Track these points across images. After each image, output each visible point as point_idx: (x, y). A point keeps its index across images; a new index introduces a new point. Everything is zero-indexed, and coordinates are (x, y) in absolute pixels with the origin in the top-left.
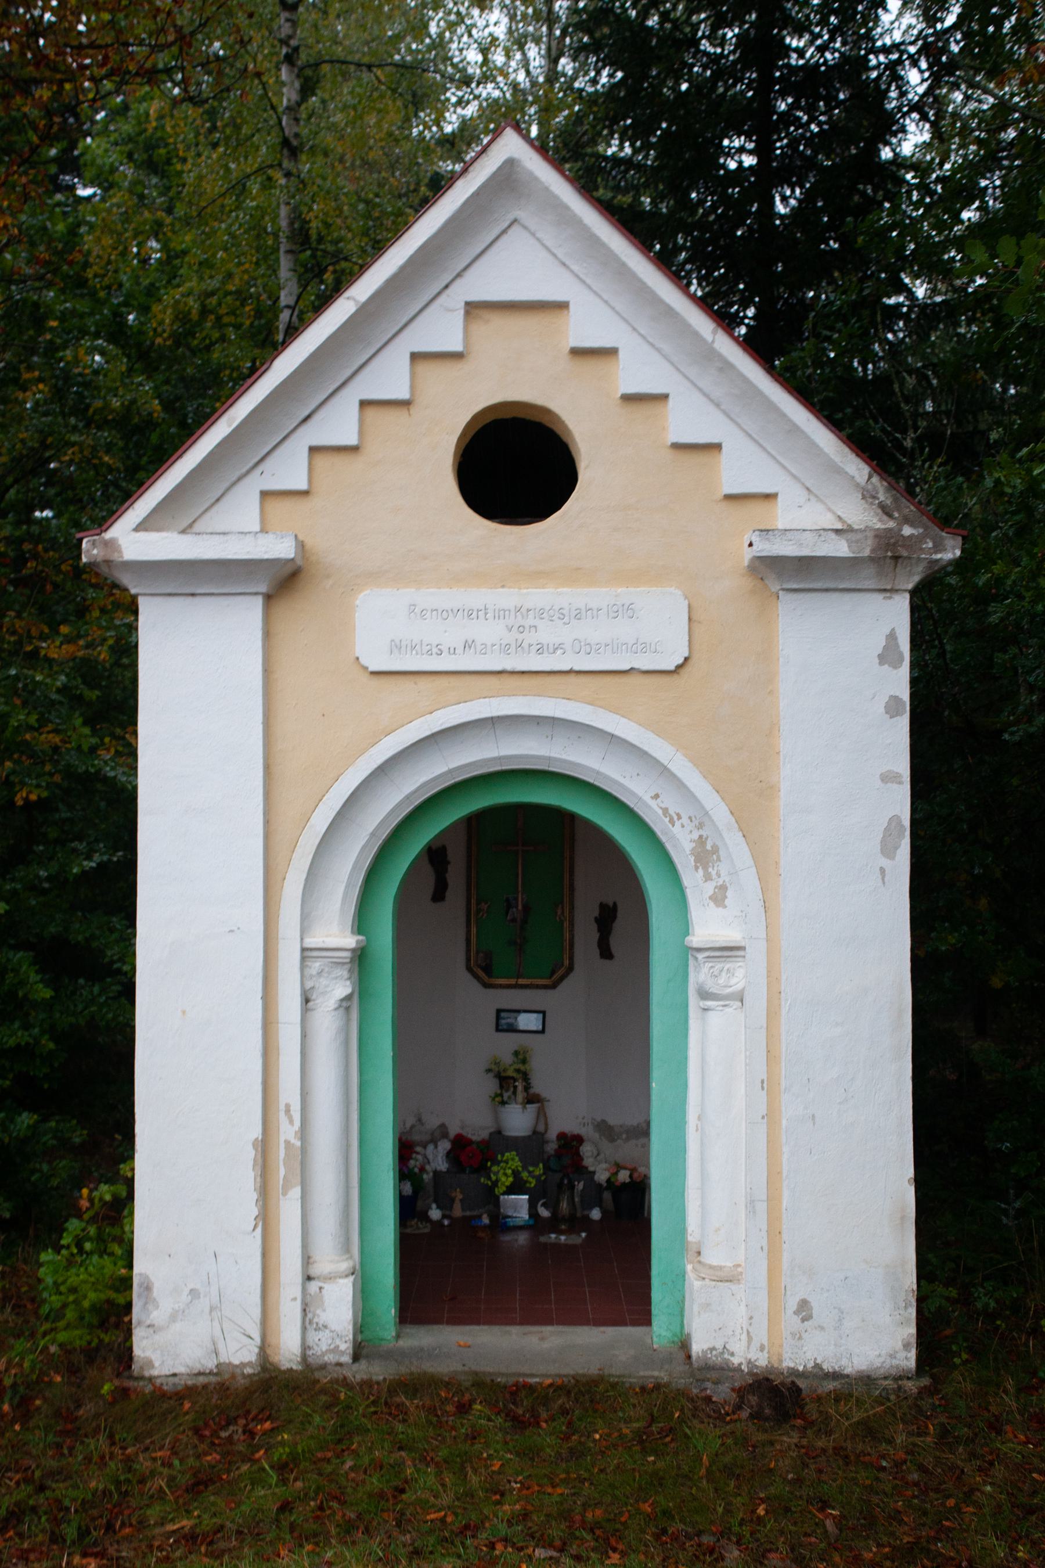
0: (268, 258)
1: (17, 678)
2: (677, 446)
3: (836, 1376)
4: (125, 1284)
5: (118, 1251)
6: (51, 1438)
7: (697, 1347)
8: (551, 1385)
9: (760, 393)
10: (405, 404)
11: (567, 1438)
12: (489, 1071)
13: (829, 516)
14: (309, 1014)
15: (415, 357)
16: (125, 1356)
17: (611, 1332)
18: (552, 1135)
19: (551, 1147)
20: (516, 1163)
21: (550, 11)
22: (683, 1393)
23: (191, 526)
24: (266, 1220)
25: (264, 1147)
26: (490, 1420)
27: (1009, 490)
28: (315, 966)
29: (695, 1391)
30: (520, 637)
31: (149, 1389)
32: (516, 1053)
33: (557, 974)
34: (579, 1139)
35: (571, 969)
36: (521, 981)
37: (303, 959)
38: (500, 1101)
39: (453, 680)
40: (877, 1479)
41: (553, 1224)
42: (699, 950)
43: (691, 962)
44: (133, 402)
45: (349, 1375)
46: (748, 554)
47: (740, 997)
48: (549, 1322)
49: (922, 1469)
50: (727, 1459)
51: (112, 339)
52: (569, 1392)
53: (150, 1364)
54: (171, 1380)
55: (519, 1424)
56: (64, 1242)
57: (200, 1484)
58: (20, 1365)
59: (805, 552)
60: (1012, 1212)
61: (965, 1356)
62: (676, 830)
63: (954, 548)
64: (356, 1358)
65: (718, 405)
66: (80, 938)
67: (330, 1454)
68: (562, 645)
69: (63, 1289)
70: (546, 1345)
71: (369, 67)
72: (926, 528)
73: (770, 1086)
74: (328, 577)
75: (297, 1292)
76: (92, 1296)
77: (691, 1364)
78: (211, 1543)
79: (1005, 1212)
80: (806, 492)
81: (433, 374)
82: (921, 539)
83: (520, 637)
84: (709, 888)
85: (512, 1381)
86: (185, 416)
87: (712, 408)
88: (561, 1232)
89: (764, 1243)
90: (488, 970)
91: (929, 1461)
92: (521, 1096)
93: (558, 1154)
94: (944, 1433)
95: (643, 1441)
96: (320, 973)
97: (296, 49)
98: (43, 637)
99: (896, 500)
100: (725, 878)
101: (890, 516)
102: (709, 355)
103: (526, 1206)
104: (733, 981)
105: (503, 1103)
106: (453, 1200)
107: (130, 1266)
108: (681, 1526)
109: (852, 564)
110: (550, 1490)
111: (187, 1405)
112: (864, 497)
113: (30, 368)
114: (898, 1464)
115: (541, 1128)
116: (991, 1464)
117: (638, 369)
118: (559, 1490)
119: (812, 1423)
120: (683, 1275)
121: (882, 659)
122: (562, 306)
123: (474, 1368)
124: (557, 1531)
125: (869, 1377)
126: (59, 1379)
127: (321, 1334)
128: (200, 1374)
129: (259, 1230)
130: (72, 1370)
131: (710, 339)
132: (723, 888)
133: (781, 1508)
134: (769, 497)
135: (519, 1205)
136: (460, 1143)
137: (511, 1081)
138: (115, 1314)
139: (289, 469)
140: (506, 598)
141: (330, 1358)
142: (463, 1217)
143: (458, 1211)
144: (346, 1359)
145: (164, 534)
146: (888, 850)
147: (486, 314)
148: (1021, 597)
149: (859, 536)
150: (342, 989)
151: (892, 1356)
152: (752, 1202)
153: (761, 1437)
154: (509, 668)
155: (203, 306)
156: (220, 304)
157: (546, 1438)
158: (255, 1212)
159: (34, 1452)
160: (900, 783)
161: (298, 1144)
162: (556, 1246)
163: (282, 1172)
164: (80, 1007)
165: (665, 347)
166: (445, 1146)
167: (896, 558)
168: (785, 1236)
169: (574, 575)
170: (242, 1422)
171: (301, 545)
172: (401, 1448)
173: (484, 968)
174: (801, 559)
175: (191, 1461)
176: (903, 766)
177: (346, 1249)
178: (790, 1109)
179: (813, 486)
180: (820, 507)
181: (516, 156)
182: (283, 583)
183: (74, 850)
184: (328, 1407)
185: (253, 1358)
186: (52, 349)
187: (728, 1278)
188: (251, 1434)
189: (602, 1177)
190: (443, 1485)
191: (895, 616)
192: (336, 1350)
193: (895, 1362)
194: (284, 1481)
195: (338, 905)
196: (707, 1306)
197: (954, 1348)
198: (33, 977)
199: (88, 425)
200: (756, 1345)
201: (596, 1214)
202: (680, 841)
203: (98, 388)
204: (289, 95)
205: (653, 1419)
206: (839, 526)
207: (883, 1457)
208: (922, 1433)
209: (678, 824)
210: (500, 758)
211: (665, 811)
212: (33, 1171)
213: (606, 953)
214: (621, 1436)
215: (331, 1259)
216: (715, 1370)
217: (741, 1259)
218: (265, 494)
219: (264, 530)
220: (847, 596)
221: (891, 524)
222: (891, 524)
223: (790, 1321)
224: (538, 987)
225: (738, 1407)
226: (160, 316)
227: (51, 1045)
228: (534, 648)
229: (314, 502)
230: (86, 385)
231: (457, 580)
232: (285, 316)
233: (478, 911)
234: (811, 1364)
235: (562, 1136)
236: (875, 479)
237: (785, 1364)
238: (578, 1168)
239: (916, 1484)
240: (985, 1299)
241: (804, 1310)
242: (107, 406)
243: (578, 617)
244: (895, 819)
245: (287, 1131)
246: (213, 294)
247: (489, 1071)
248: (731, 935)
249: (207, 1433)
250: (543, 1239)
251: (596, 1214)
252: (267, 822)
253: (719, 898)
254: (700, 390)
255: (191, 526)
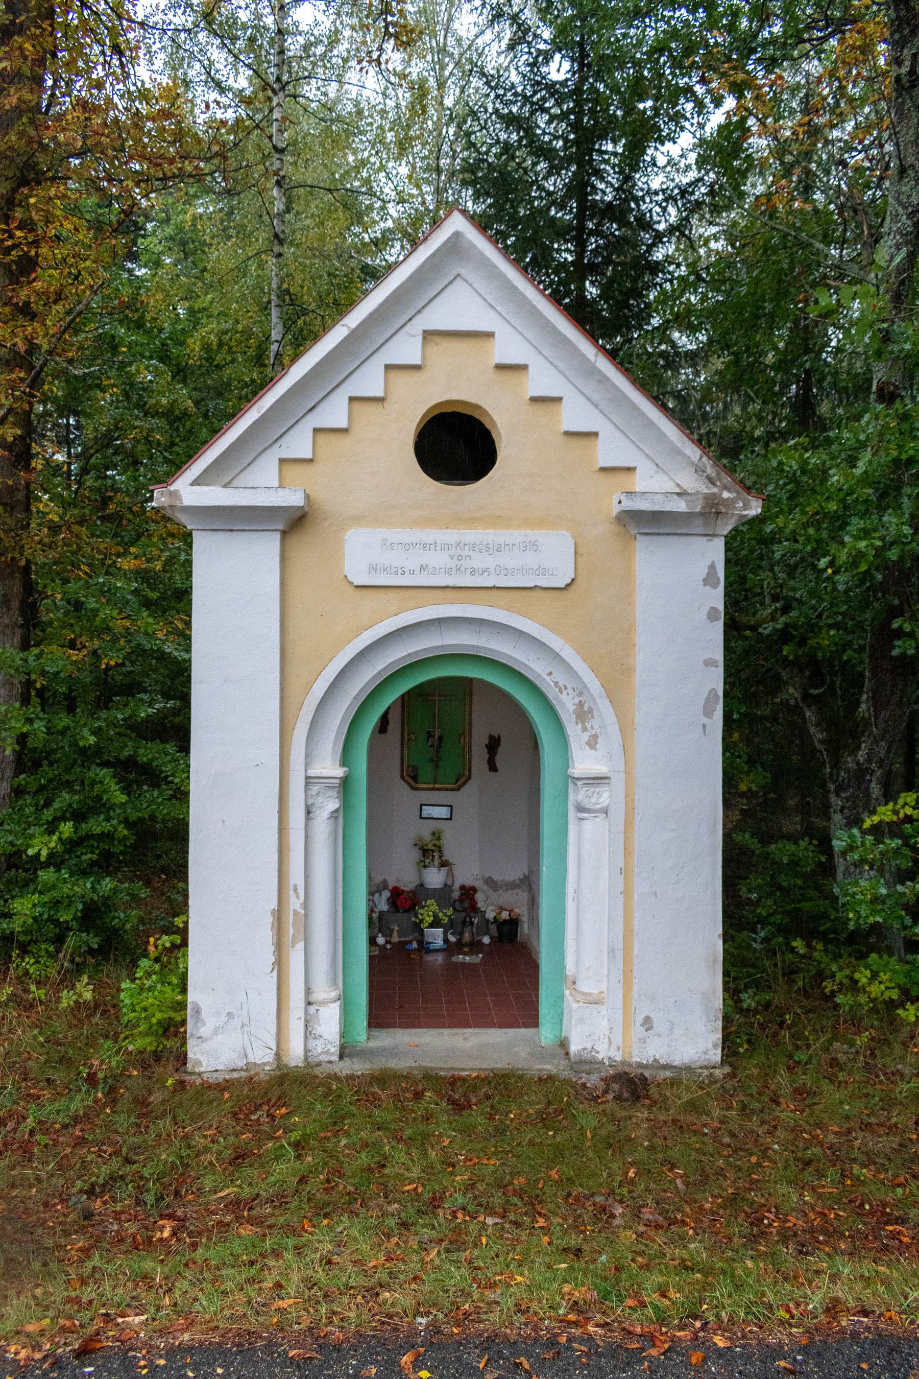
0: (266, 308)
1: (103, 584)
2: (567, 434)
3: (666, 1067)
4: (182, 1006)
5: (175, 981)
6: (132, 1120)
7: (574, 1048)
8: (477, 1077)
9: (627, 398)
10: (381, 400)
11: (491, 1118)
12: (416, 845)
13: (672, 484)
14: (310, 822)
15: (388, 367)
16: (182, 1058)
17: (511, 1032)
18: (457, 887)
19: (456, 895)
20: (435, 907)
21: (438, 165)
22: (566, 1081)
23: (230, 482)
24: (280, 964)
25: (279, 915)
26: (437, 1104)
27: (787, 469)
28: (315, 789)
29: (574, 1079)
30: (459, 563)
31: (199, 1081)
32: (434, 834)
33: (460, 781)
34: (474, 890)
35: (469, 778)
36: (438, 786)
37: (307, 784)
38: (423, 865)
39: (517, 593)
40: (703, 1143)
41: (459, 947)
42: (579, 779)
43: (571, 786)
44: (175, 401)
45: (337, 1070)
46: (616, 509)
47: (605, 811)
48: (468, 1026)
49: (733, 1135)
50: (603, 1132)
51: (161, 360)
52: (490, 1083)
53: (199, 1063)
54: (215, 1075)
55: (459, 1107)
56: (137, 975)
57: (239, 1158)
58: (110, 1062)
59: (657, 508)
60: (759, 940)
61: (746, 1046)
62: (564, 697)
63: (756, 507)
64: (341, 1057)
65: (596, 406)
66: (145, 759)
67: (329, 1134)
68: (488, 569)
69: (137, 1008)
70: (469, 1044)
71: (330, 190)
72: (738, 493)
73: (626, 872)
74: (326, 519)
75: (301, 1014)
76: (159, 1016)
77: (570, 1059)
78: (251, 1209)
79: (755, 940)
80: (654, 467)
81: (401, 380)
82: (734, 501)
83: (459, 563)
84: (586, 737)
85: (450, 1074)
86: (208, 411)
87: (592, 408)
88: (465, 954)
89: (621, 978)
90: (415, 778)
91: (735, 1128)
92: (436, 862)
93: (461, 900)
94: (744, 1107)
95: (544, 1120)
96: (318, 794)
97: (284, 177)
98: (118, 555)
99: (718, 473)
100: (597, 730)
101: (714, 484)
102: (592, 371)
103: (441, 935)
104: (601, 800)
105: (425, 867)
106: (392, 931)
107: (184, 990)
108: (580, 1189)
109: (688, 517)
110: (486, 1162)
111: (227, 1095)
112: (696, 471)
113: (108, 378)
114: (715, 1131)
115: (449, 882)
116: (775, 1127)
117: (542, 379)
118: (492, 1162)
119: (655, 1102)
120: (562, 997)
121: (706, 582)
122: (490, 335)
123: (424, 1064)
124: (497, 1200)
125: (690, 1068)
126: (136, 1073)
127: (317, 1042)
128: (234, 1070)
129: (275, 972)
130: (145, 1066)
131: (593, 359)
132: (595, 737)
133: (644, 1171)
134: (631, 470)
135: (448, 946)
136: (396, 893)
137: (430, 852)
138: (174, 1027)
139: (299, 444)
140: (450, 536)
141: (324, 1058)
142: (400, 942)
143: (395, 938)
144: (335, 1058)
145: (212, 488)
146: (708, 713)
147: (437, 339)
148: (796, 541)
149: (693, 498)
150: (333, 804)
151: (705, 1053)
152: (613, 950)
153: (623, 1114)
154: (451, 584)
155: (220, 340)
156: (231, 339)
157: (477, 1117)
158: (273, 959)
159: (120, 1130)
160: (717, 666)
161: (303, 912)
162: (463, 964)
163: (291, 931)
164: (145, 806)
165: (561, 365)
166: (386, 894)
167: (718, 513)
168: (635, 974)
169: (496, 521)
170: (266, 1108)
171: (307, 497)
172: (379, 1129)
173: (412, 777)
174: (654, 513)
175: (232, 1139)
176: (719, 655)
177: (334, 982)
178: (640, 888)
179: (665, 466)
180: (665, 478)
181: (460, 230)
182: (294, 523)
183: (141, 700)
184: (325, 1096)
185: (269, 1057)
186: (123, 365)
187: (596, 1001)
188: (272, 1117)
189: (490, 915)
190: (412, 1161)
191: (714, 552)
192: (327, 1052)
193: (707, 1057)
194: (299, 1157)
195: (330, 746)
196: (581, 1020)
197: (738, 1041)
198: (114, 787)
199: (145, 415)
200: (614, 1046)
201: (486, 940)
202: (566, 704)
203: (152, 391)
204: (279, 206)
205: (549, 1103)
206: (678, 490)
207: (705, 1125)
208: (730, 1108)
209: (565, 692)
210: (443, 646)
211: (556, 684)
212: (113, 918)
213: (493, 768)
214: (529, 1115)
215: (324, 991)
216: (587, 1063)
217: (604, 987)
218: (282, 461)
219: (281, 486)
220: (683, 539)
221: (715, 490)
222: (715, 490)
223: (638, 1030)
224: (447, 789)
225: (606, 1092)
226: (192, 346)
227: (126, 832)
228: (469, 571)
229: (318, 468)
230: (144, 389)
231: (416, 523)
232: (274, 347)
233: (409, 739)
234: (651, 1060)
235: (463, 887)
236: (705, 459)
237: (634, 1059)
238: (474, 907)
239: (729, 1146)
240: (749, 1001)
241: (647, 1023)
242: (158, 402)
243: (499, 550)
244: (713, 691)
245: (295, 904)
246: (226, 332)
247: (416, 845)
248: (600, 769)
249: (242, 1116)
250: (454, 959)
251: (486, 940)
252: (282, 690)
253: (592, 743)
254: (584, 395)
255: (230, 482)
